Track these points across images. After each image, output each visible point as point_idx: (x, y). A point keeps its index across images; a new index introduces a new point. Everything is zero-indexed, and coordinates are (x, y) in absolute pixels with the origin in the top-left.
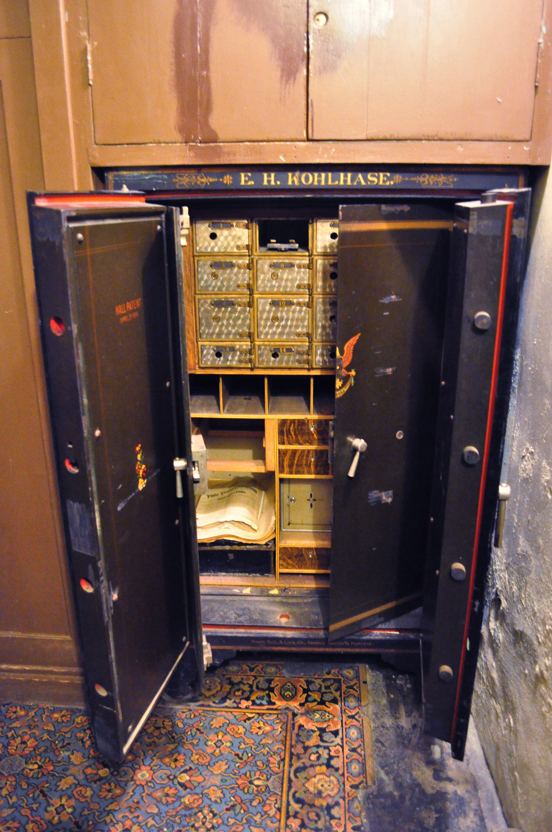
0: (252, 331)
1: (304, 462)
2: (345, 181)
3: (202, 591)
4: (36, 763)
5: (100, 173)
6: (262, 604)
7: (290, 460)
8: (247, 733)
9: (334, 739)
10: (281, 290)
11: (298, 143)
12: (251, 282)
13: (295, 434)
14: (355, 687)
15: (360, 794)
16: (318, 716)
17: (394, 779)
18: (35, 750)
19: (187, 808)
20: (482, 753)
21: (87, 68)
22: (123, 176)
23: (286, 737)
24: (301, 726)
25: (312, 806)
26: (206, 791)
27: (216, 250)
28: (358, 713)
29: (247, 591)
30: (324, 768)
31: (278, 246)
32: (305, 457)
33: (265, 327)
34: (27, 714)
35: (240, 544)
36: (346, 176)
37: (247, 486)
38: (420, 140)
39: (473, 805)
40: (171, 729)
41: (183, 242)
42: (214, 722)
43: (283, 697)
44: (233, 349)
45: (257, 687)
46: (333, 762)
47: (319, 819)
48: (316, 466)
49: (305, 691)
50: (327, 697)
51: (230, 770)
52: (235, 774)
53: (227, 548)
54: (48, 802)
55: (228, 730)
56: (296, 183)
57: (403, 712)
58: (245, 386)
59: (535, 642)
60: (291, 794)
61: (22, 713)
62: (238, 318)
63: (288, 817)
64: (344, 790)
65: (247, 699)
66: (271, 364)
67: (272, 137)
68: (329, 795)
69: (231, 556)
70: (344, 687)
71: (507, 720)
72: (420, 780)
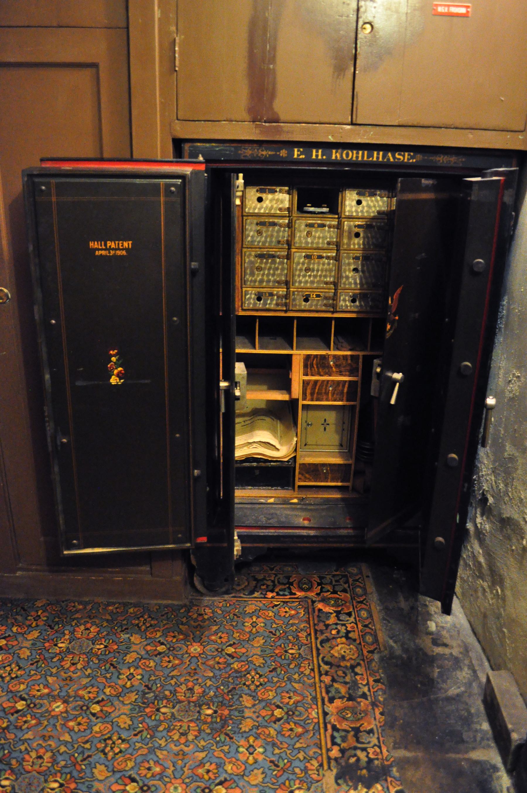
0: (288, 279)
1: (324, 391)
2: (378, 158)
3: (236, 501)
4: (102, 644)
5: (178, 144)
7: (312, 389)
8: (276, 616)
9: (348, 618)
10: (315, 246)
11: (345, 126)
12: (290, 239)
13: (317, 367)
14: (360, 580)
15: (376, 657)
16: (333, 602)
18: (98, 634)
19: (236, 671)
20: (469, 626)
21: (175, 57)
22: (197, 147)
23: (309, 618)
24: (320, 610)
25: (339, 666)
26: (250, 659)
28: (365, 599)
29: (272, 500)
30: (344, 640)
31: (312, 209)
32: (324, 387)
34: (85, 608)
35: (266, 461)
36: (378, 154)
38: (441, 128)
39: (467, 662)
40: (212, 615)
41: (238, 202)
42: (247, 609)
43: (302, 589)
44: (271, 294)
45: (279, 582)
46: (351, 635)
47: (346, 675)
48: (333, 394)
51: (267, 643)
52: (272, 646)
53: (255, 464)
54: (119, 672)
55: (260, 614)
57: (402, 599)
58: (278, 328)
60: (320, 658)
62: (277, 269)
63: (320, 675)
64: (363, 654)
65: (272, 591)
66: (303, 307)
68: (351, 659)
70: (351, 580)
71: (494, 591)
72: (422, 646)
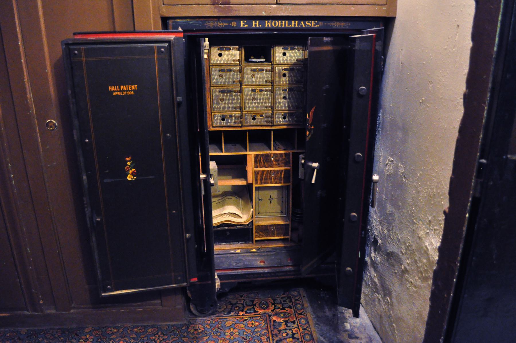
2: (295, 25)
3: (215, 253)
5: (165, 20)
6: (248, 259)
13: (264, 162)
17: (329, 340)
22: (178, 22)
24: (274, 321)
27: (222, 62)
29: (239, 251)
30: (291, 339)
31: (254, 60)
33: (248, 103)
34: (118, 331)
36: (295, 22)
37: (232, 196)
41: (206, 56)
43: (262, 308)
44: (231, 116)
45: (246, 305)
46: (295, 336)
49: (273, 304)
50: (285, 306)
53: (226, 228)
56: (270, 26)
58: (236, 138)
59: (400, 254)
61: (115, 330)
62: (234, 99)
65: (242, 311)
66: (252, 124)
67: (258, 2)
69: (228, 233)
